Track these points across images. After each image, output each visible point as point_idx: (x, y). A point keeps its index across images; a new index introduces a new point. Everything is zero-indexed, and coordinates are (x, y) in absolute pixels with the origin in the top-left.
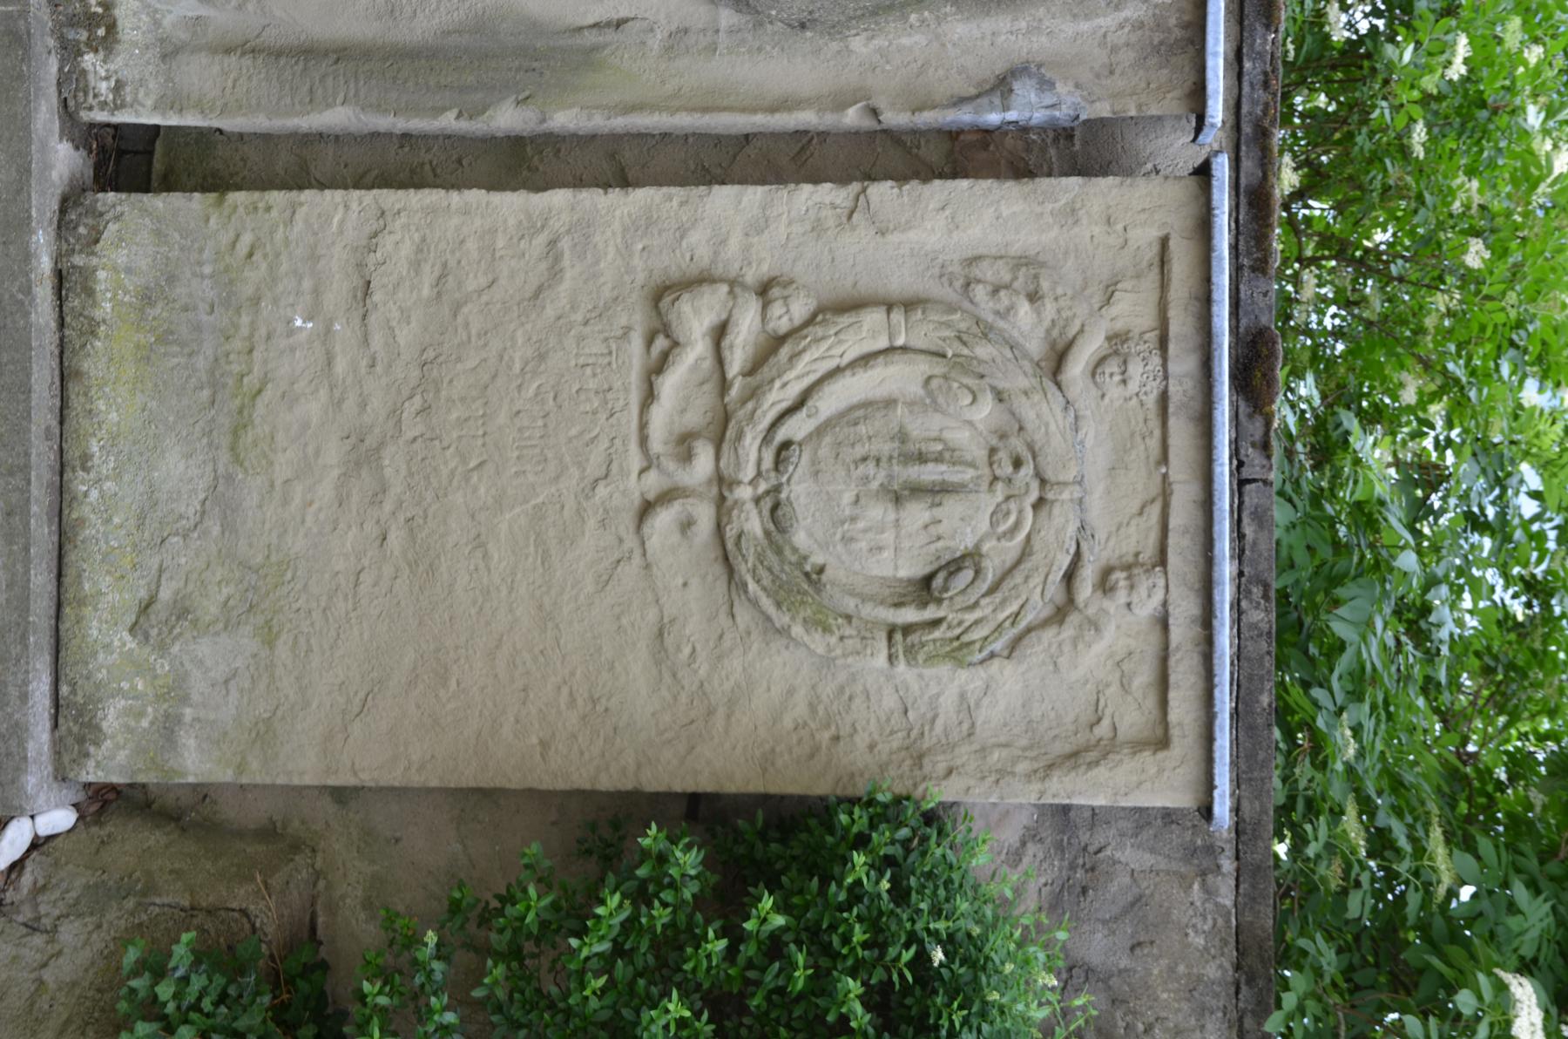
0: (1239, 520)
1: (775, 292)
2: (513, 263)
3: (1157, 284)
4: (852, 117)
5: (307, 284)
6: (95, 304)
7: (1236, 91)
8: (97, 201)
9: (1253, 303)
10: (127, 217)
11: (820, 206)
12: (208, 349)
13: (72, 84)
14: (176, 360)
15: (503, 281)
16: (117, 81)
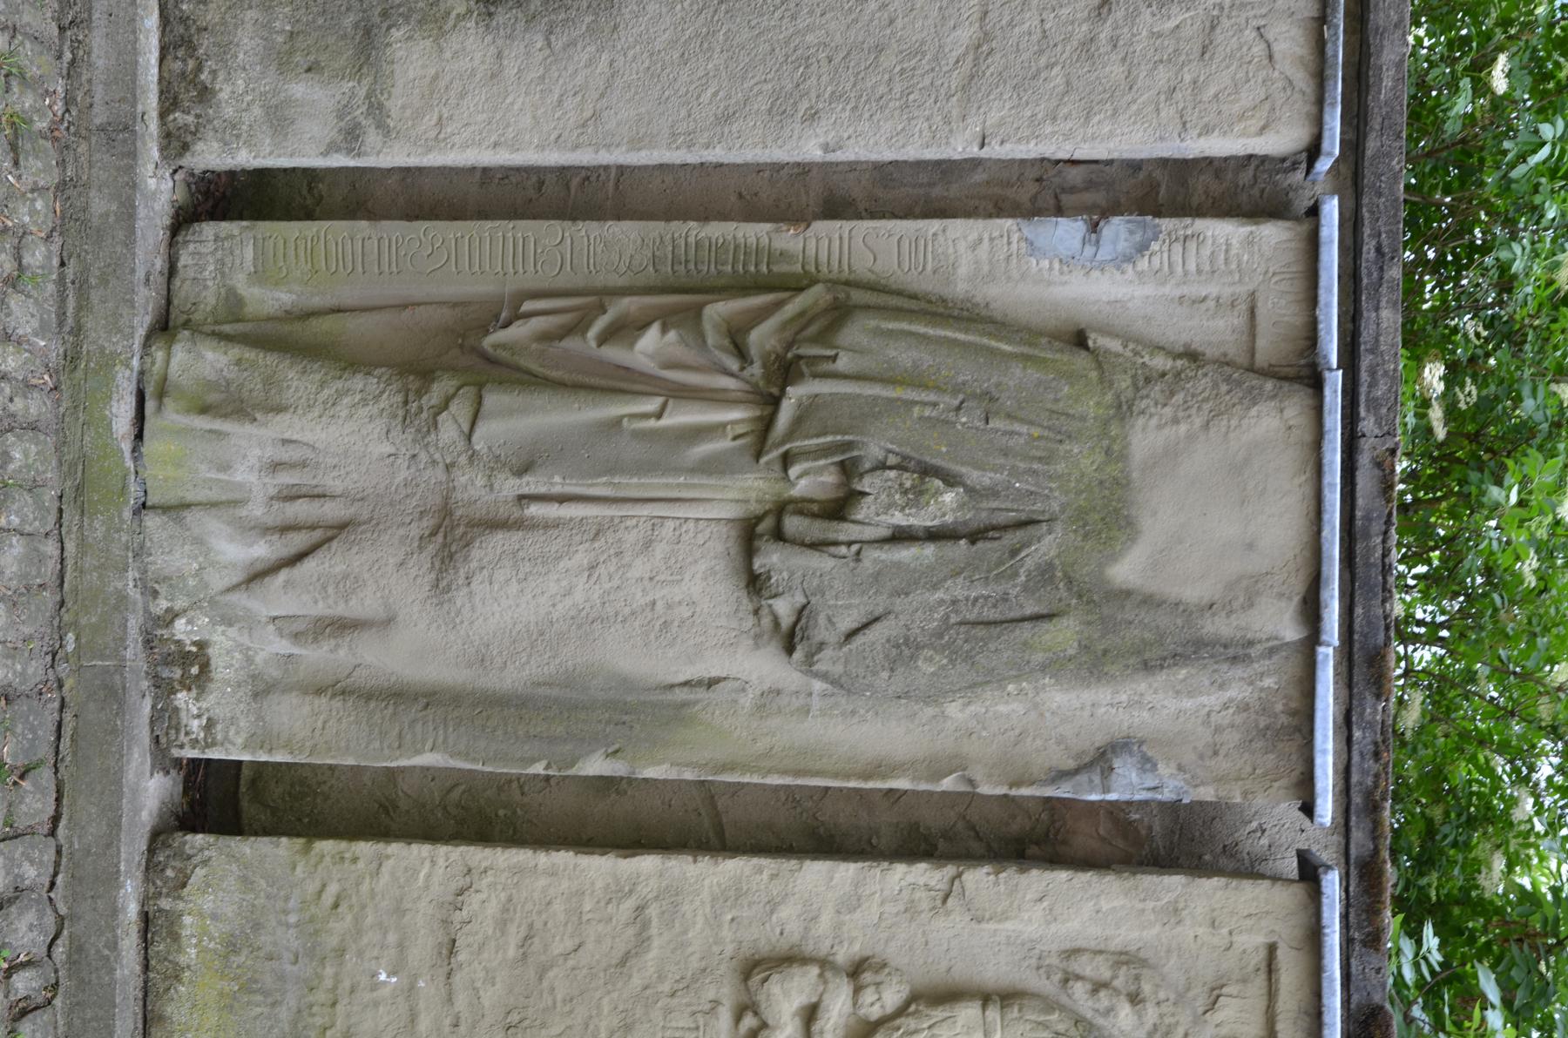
0: (1348, 959)
1: (867, 977)
2: (600, 928)
3: (1264, 991)
4: (948, 784)
5: (392, 938)
6: (180, 950)
7: (1345, 756)
8: (185, 843)
9: (1365, 979)
10: (214, 863)
11: (914, 887)
12: (291, 1001)
13: (165, 719)
14: (259, 1010)
15: (590, 946)
16: (209, 719)
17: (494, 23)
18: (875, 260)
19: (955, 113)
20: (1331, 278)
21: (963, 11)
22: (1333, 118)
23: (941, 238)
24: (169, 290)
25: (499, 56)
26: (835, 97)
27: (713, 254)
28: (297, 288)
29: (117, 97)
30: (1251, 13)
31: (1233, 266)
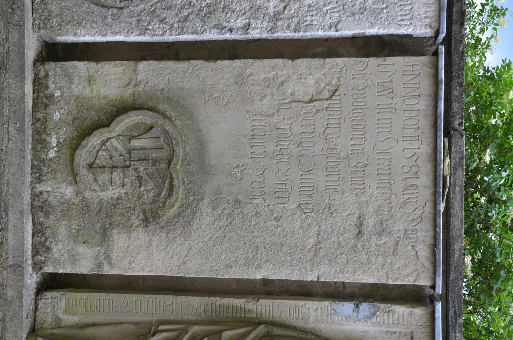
17: (149, 229)
18: (281, 314)
19: (309, 268)
20: (439, 331)
21: (311, 233)
22: (439, 280)
23: (304, 307)
24: (35, 316)
25: (150, 240)
26: (267, 261)
27: (225, 309)
28: (80, 316)
29: (17, 255)
30: (410, 241)
31: (405, 322)
